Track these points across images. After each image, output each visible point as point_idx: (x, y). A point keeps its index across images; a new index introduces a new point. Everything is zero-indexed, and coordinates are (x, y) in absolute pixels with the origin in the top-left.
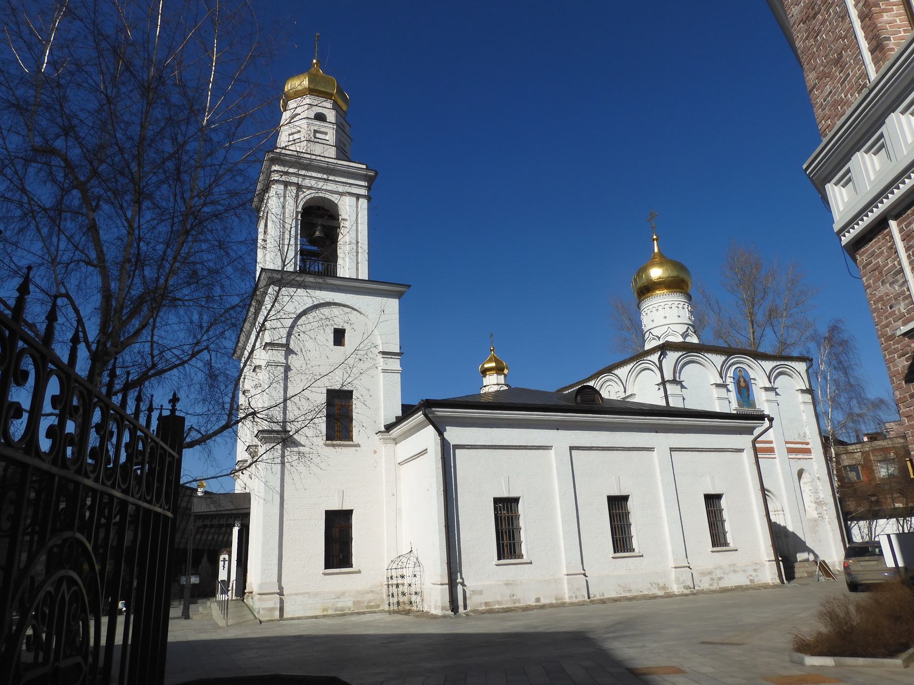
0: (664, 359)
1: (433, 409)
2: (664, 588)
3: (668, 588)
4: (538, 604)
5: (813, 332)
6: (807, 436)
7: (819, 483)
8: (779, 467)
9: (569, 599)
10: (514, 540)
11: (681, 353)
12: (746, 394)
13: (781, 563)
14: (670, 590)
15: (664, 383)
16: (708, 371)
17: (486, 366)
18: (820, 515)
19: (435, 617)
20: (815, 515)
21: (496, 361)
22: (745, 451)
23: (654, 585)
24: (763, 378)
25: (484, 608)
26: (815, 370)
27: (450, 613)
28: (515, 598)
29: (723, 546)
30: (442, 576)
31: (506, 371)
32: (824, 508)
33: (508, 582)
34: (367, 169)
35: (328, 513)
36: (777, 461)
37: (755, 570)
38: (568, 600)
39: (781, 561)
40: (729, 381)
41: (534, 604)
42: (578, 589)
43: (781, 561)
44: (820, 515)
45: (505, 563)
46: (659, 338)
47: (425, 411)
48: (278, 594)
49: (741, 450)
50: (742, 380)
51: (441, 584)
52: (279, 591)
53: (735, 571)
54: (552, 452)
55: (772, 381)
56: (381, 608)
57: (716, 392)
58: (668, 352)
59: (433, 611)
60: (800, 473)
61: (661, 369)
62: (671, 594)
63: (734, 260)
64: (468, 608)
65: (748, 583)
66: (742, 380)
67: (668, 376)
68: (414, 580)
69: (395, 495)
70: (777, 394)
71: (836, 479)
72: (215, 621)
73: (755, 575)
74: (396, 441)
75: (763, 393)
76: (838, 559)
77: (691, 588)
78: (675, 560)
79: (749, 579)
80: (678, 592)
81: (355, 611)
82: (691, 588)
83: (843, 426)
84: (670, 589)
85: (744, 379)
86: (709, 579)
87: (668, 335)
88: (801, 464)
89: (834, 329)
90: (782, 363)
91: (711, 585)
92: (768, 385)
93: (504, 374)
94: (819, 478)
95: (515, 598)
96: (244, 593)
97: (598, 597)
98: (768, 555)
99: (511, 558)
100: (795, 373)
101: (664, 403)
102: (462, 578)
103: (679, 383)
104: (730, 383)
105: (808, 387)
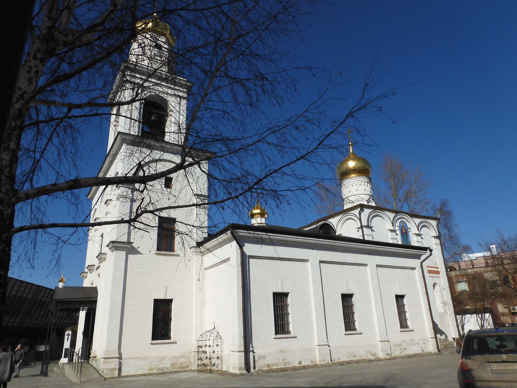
1: (237, 230)
11: (371, 210)
12: (406, 237)
14: (378, 356)
15: (362, 227)
19: (234, 375)
20: (442, 310)
21: (260, 209)
22: (416, 269)
23: (369, 353)
25: (266, 368)
27: (245, 372)
30: (239, 346)
31: (266, 216)
32: (447, 307)
34: (187, 81)
35: (155, 301)
37: (424, 343)
38: (319, 363)
41: (298, 365)
42: (325, 355)
46: (353, 202)
47: (232, 231)
48: (118, 358)
49: (414, 269)
51: (239, 352)
52: (119, 356)
53: (413, 344)
54: (309, 264)
56: (189, 368)
57: (389, 233)
58: (364, 209)
59: (232, 371)
61: (360, 220)
62: (379, 359)
65: (421, 352)
66: (403, 228)
67: (365, 223)
68: (215, 348)
69: (202, 290)
70: (372, 230)
72: (67, 378)
74: (203, 254)
75: (415, 237)
77: (390, 355)
78: (381, 337)
80: (383, 357)
81: (172, 370)
85: (405, 228)
87: (358, 201)
88: (435, 280)
89: (443, 204)
90: (424, 220)
91: (400, 353)
92: (417, 232)
93: (265, 217)
94: (444, 289)
96: (89, 358)
97: (336, 361)
99: (283, 334)
101: (362, 238)
102: (252, 347)
103: (370, 228)
105: (438, 235)
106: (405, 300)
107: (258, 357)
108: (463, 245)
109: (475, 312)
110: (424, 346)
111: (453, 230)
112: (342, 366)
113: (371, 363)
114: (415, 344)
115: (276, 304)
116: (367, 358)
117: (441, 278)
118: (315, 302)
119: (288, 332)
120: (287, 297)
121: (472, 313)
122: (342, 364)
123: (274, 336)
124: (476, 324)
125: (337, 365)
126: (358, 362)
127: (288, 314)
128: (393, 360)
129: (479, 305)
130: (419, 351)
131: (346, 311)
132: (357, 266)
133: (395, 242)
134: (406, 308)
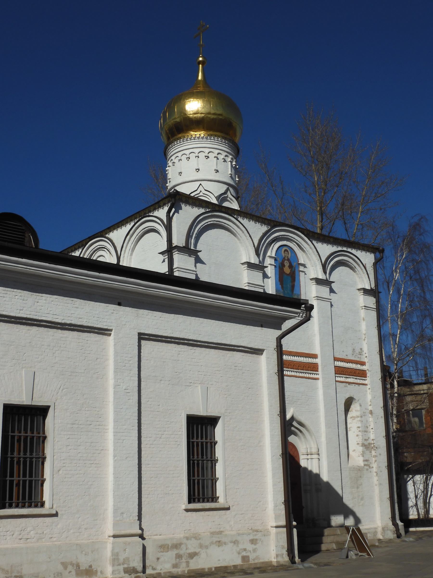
0: (176, 214)
3: (96, 571)
6: (364, 353)
7: (371, 419)
8: (320, 392)
11: (202, 210)
12: (289, 285)
13: (295, 531)
16: (241, 243)
18: (367, 464)
22: (265, 353)
23: (70, 568)
24: (316, 266)
26: (387, 279)
32: (373, 453)
36: (320, 383)
37: (253, 542)
39: (295, 527)
43: (295, 527)
44: (366, 463)
45: (16, 514)
49: (258, 352)
50: (287, 264)
53: (219, 543)
54: (110, 340)
55: (328, 272)
58: (183, 206)
60: (348, 403)
61: (169, 228)
63: (309, 130)
65: (238, 561)
66: (287, 264)
70: (332, 291)
71: (395, 421)
73: (251, 550)
76: (382, 523)
78: (115, 525)
79: (240, 556)
82: (137, 572)
83: (411, 353)
84: (99, 573)
85: (290, 263)
86: (174, 556)
90: (345, 249)
91: (175, 566)
92: (321, 276)
94: (371, 412)
98: (277, 518)
99: (23, 507)
100: (358, 265)
104: (269, 266)
105: (373, 286)
110: (253, 546)
114: (225, 543)
117: (368, 386)
131: (198, 455)
132: (75, 333)
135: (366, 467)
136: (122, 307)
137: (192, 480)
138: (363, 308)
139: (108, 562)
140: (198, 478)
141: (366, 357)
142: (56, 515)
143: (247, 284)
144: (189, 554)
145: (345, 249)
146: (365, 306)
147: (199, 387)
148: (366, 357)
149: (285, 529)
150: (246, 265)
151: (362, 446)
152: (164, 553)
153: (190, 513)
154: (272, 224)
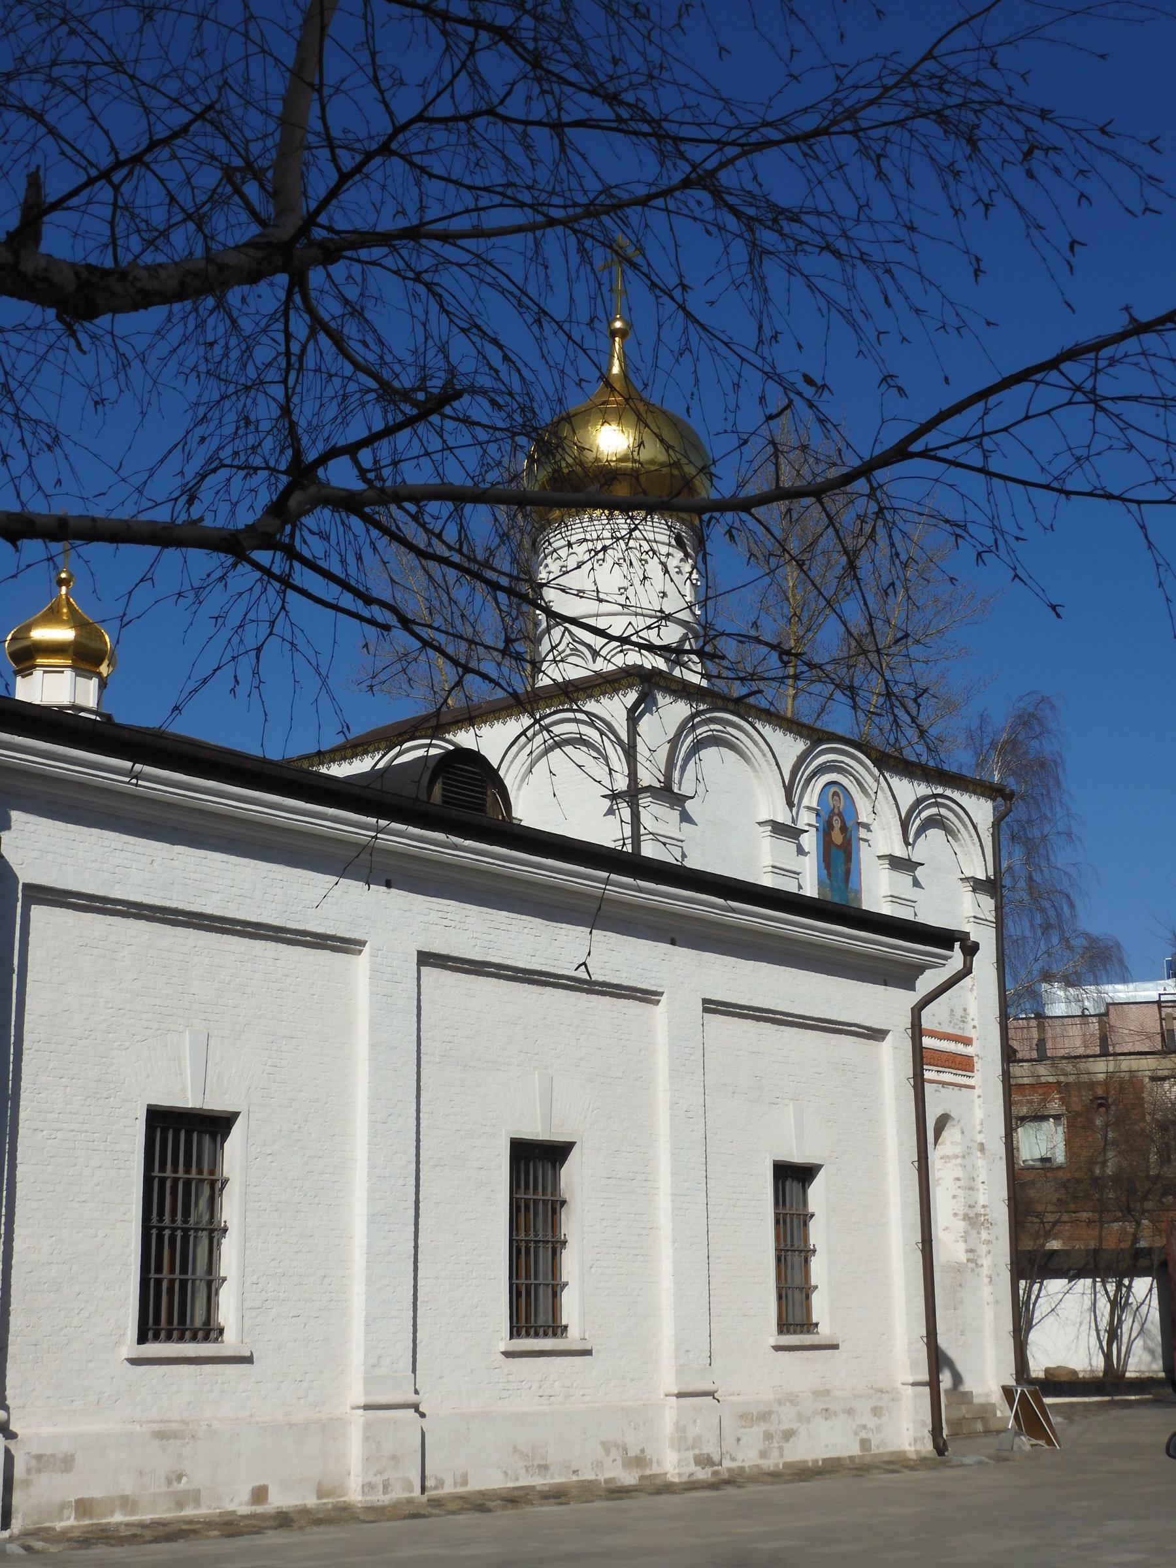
2: (640, 1461)
4: (259, 1509)
5: (977, 721)
6: (969, 1019)
7: (980, 1162)
9: (364, 1493)
10: (184, 1270)
12: (841, 870)
14: (655, 1470)
17: (42, 634)
21: (76, 621)
22: (889, 1037)
25: (72, 1522)
28: (184, 1484)
29: (546, 1335)
31: (104, 669)
32: (984, 1235)
33: (162, 1426)
37: (876, 1411)
38: (360, 1498)
40: (806, 819)
41: (245, 1510)
42: (394, 1458)
45: (537, 1348)
49: (877, 1034)
50: (837, 824)
54: (362, 963)
61: (630, 752)
62: (658, 1481)
64: (13, 1521)
65: (855, 1450)
66: (837, 824)
70: (685, 817)
78: (680, 1372)
79: (858, 1438)
80: (680, 1475)
84: (655, 1465)
86: (762, 1435)
90: (940, 790)
91: (764, 1454)
92: (899, 851)
93: (99, 675)
94: (982, 1148)
95: (184, 1484)
97: (449, 1489)
98: (914, 1365)
103: (675, 800)
105: (991, 872)
106: (817, 1192)
107: (33, 1463)
108: (1087, 936)
109: (1091, 1266)
111: (1052, 858)
112: (477, 1515)
113: (626, 1503)
115: (156, 1173)
116: (601, 1478)
117: (977, 1092)
118: (370, 1174)
119: (210, 1331)
120: (223, 1141)
121: (1073, 1273)
122: (479, 1503)
123: (129, 1345)
124: (1085, 1327)
125: (453, 1513)
126: (557, 1495)
127: (216, 1232)
128: (730, 1491)
129: (1116, 1232)
130: (847, 1447)
133: (789, 886)
134: (817, 1234)
135: (972, 1265)
136: (676, 948)
137: (152, 1282)
138: (972, 919)
139: (667, 1443)
140: (172, 1276)
141: (974, 1027)
142: (587, 1353)
143: (770, 869)
144: (783, 1432)
145: (940, 790)
146: (773, 867)
147: (791, 1106)
148: (974, 1027)
149: (927, 1389)
150: (770, 828)
151: (964, 1219)
152: (747, 1430)
153: (780, 1353)
154: (815, 737)
